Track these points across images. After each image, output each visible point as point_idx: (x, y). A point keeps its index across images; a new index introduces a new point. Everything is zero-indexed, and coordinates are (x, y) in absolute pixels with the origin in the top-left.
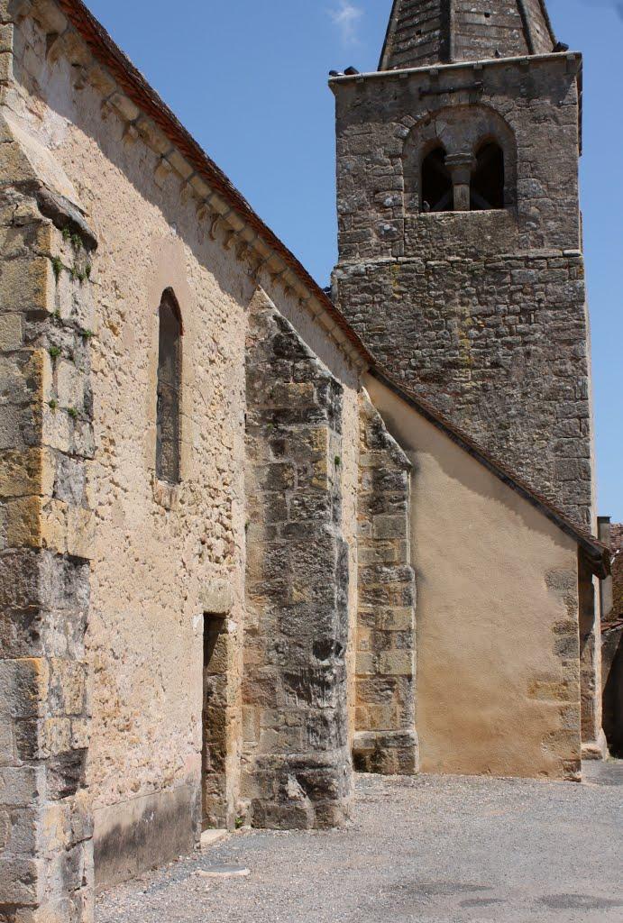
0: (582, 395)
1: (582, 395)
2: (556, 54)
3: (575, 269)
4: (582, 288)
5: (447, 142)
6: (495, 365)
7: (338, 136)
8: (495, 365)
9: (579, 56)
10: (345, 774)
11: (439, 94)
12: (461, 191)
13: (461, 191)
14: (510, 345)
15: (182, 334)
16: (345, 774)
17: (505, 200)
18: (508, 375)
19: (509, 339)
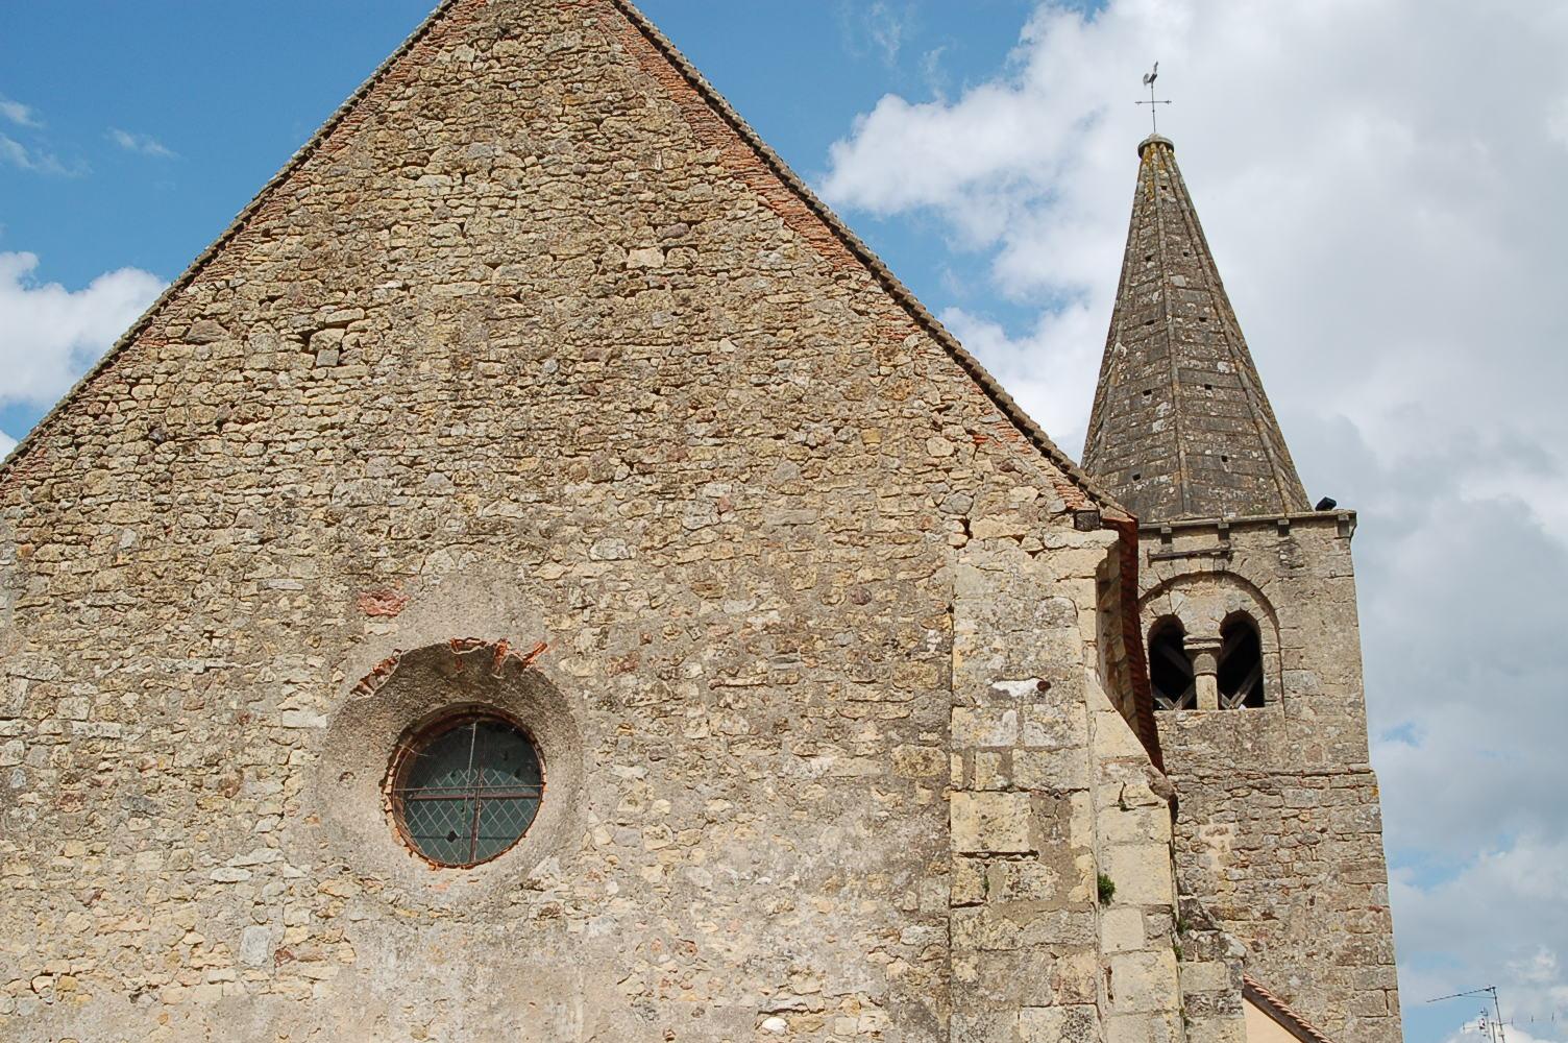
0: (1388, 959)
1: (1388, 959)
2: (1320, 512)
3: (1365, 793)
4: (1377, 815)
5: (1185, 619)
6: (1268, 916)
7: (1359, 654)
8: (1268, 916)
9: (1353, 516)
10: (288, 625)
11: (1173, 557)
12: (1206, 686)
13: (1206, 686)
14: (1285, 889)
15: (438, 646)
16: (288, 625)
17: (1266, 697)
18: (1286, 928)
19: (1285, 881)
